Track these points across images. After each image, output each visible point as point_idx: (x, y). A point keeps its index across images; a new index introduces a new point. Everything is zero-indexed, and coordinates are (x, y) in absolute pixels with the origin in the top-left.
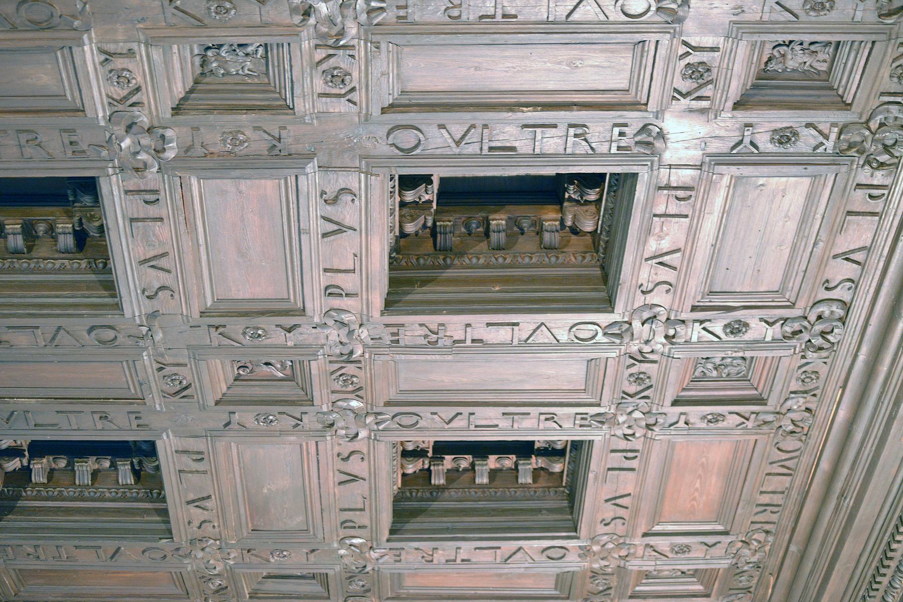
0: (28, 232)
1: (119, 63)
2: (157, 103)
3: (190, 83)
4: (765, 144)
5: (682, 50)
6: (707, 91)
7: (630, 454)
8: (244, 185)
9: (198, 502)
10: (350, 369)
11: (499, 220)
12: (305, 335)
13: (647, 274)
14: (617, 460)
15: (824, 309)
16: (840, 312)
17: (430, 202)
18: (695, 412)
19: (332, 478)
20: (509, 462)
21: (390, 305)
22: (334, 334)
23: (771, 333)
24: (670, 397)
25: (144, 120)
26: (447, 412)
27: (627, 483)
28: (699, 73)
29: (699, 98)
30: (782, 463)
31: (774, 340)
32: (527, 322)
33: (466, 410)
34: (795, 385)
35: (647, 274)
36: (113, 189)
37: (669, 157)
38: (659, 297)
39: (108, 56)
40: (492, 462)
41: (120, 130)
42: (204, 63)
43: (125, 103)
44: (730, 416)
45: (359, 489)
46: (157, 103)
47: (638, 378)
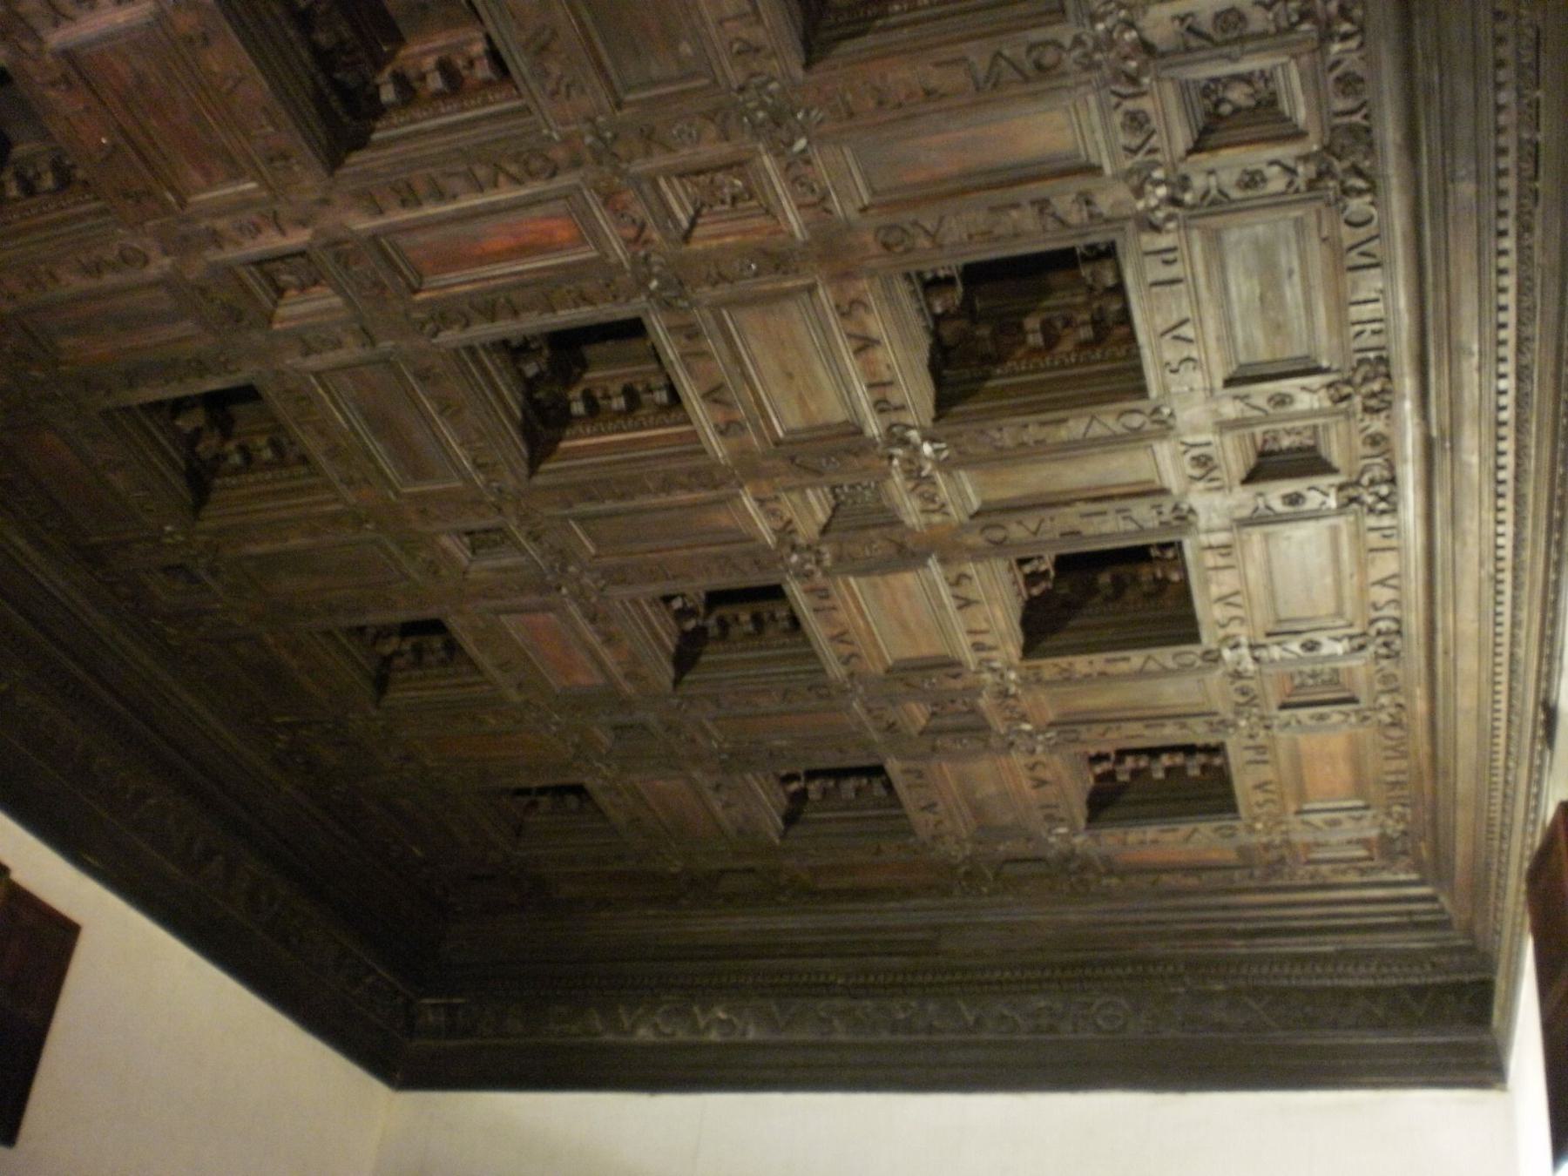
0: (757, 619)
1: (771, 505)
2: (807, 530)
3: (829, 512)
4: (1278, 506)
5: (1182, 448)
6: (1215, 474)
7: (1260, 749)
8: (891, 578)
9: (931, 807)
10: (1011, 702)
11: (1105, 579)
12: (969, 679)
13: (1219, 612)
14: (1250, 755)
15: (1382, 625)
16: (1393, 626)
17: (1046, 572)
18: (1304, 713)
19: (1026, 785)
20: (1143, 762)
21: (1029, 650)
22: (987, 677)
23: (1340, 648)
24: (1274, 701)
25: (801, 541)
26: (1099, 728)
27: (1267, 773)
28: (1204, 462)
29: (1212, 480)
30: (1393, 748)
31: (1345, 653)
32: (1136, 658)
33: (1113, 725)
34: (1378, 687)
35: (1219, 612)
36: (795, 589)
37: (1202, 523)
38: (1233, 629)
39: (761, 502)
40: (1166, 760)
41: (787, 549)
42: (836, 496)
43: (786, 531)
44: (1335, 714)
45: (1050, 790)
46: (807, 530)
47: (1244, 692)
